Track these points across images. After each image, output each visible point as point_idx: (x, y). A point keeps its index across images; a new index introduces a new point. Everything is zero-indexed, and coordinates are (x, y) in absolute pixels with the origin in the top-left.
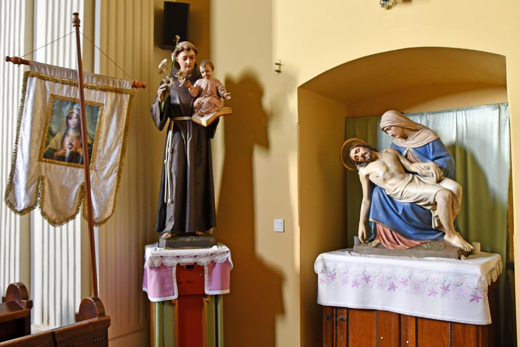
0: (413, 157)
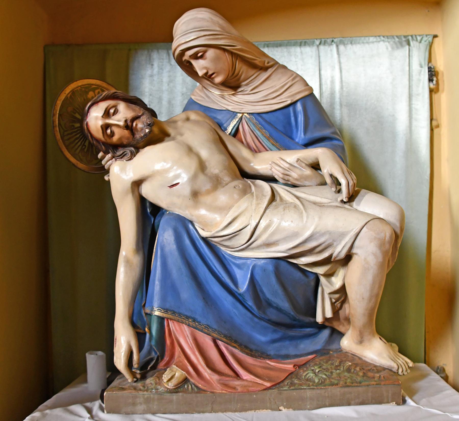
0: (254, 136)
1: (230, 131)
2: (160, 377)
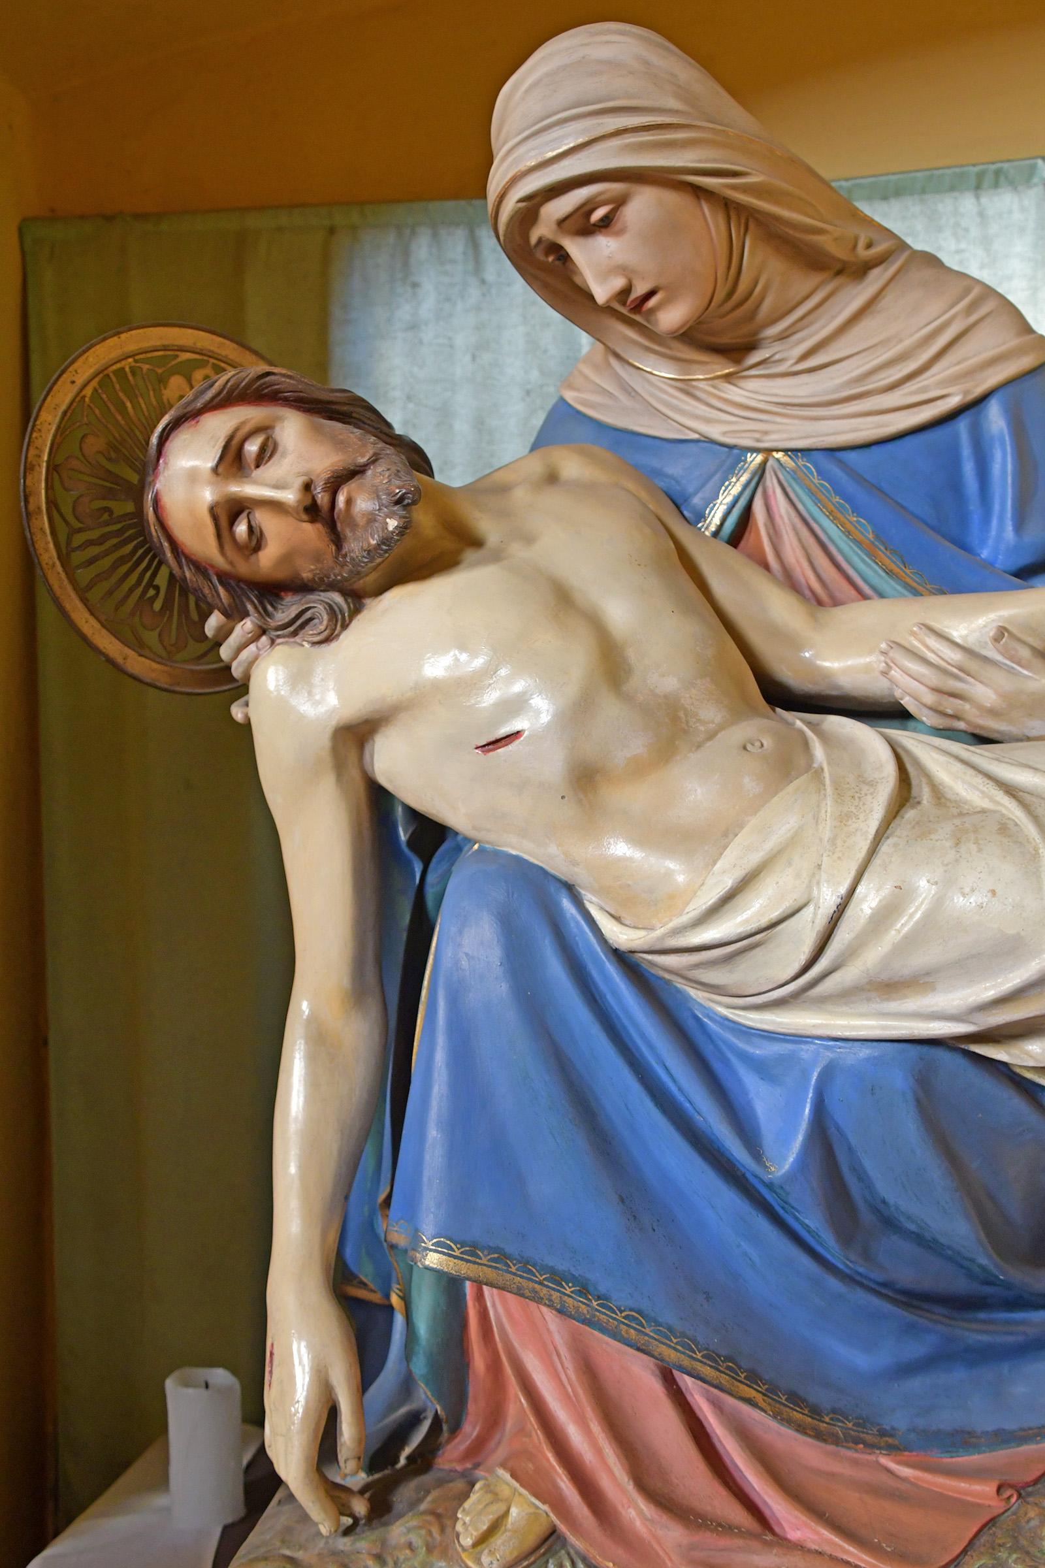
1: (717, 521)
2: (444, 1518)
